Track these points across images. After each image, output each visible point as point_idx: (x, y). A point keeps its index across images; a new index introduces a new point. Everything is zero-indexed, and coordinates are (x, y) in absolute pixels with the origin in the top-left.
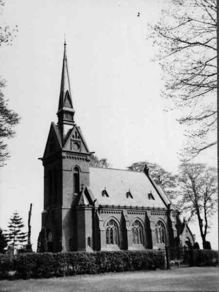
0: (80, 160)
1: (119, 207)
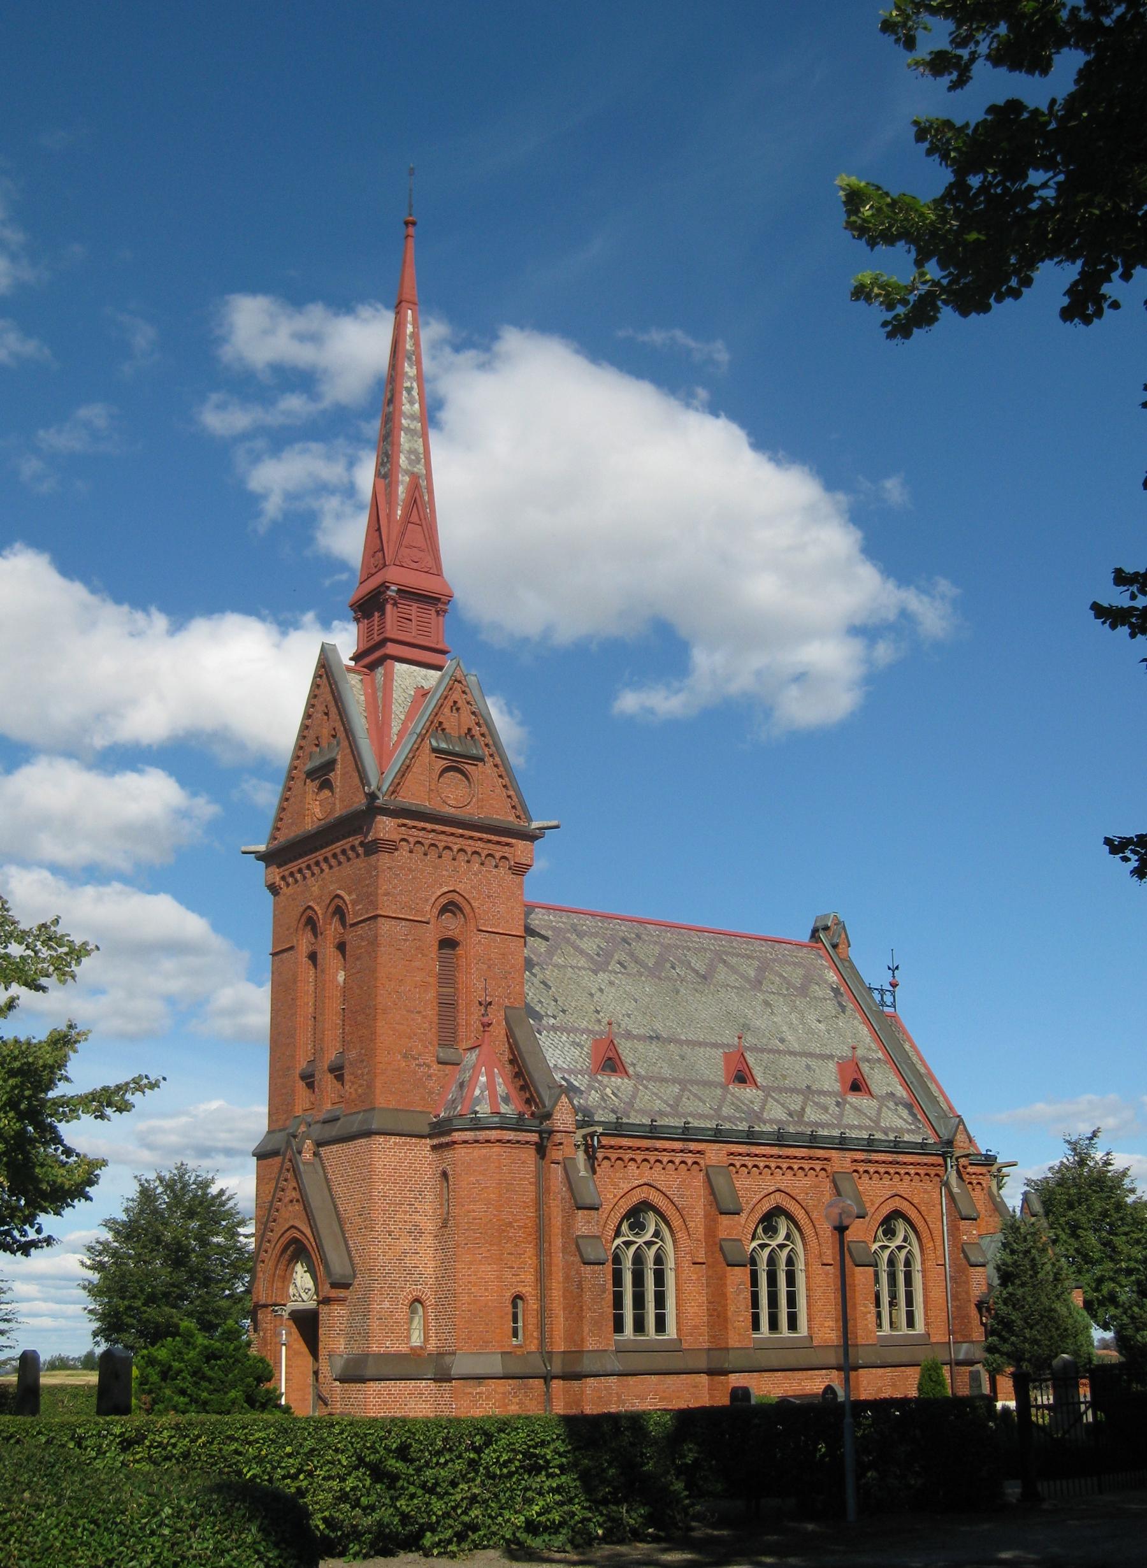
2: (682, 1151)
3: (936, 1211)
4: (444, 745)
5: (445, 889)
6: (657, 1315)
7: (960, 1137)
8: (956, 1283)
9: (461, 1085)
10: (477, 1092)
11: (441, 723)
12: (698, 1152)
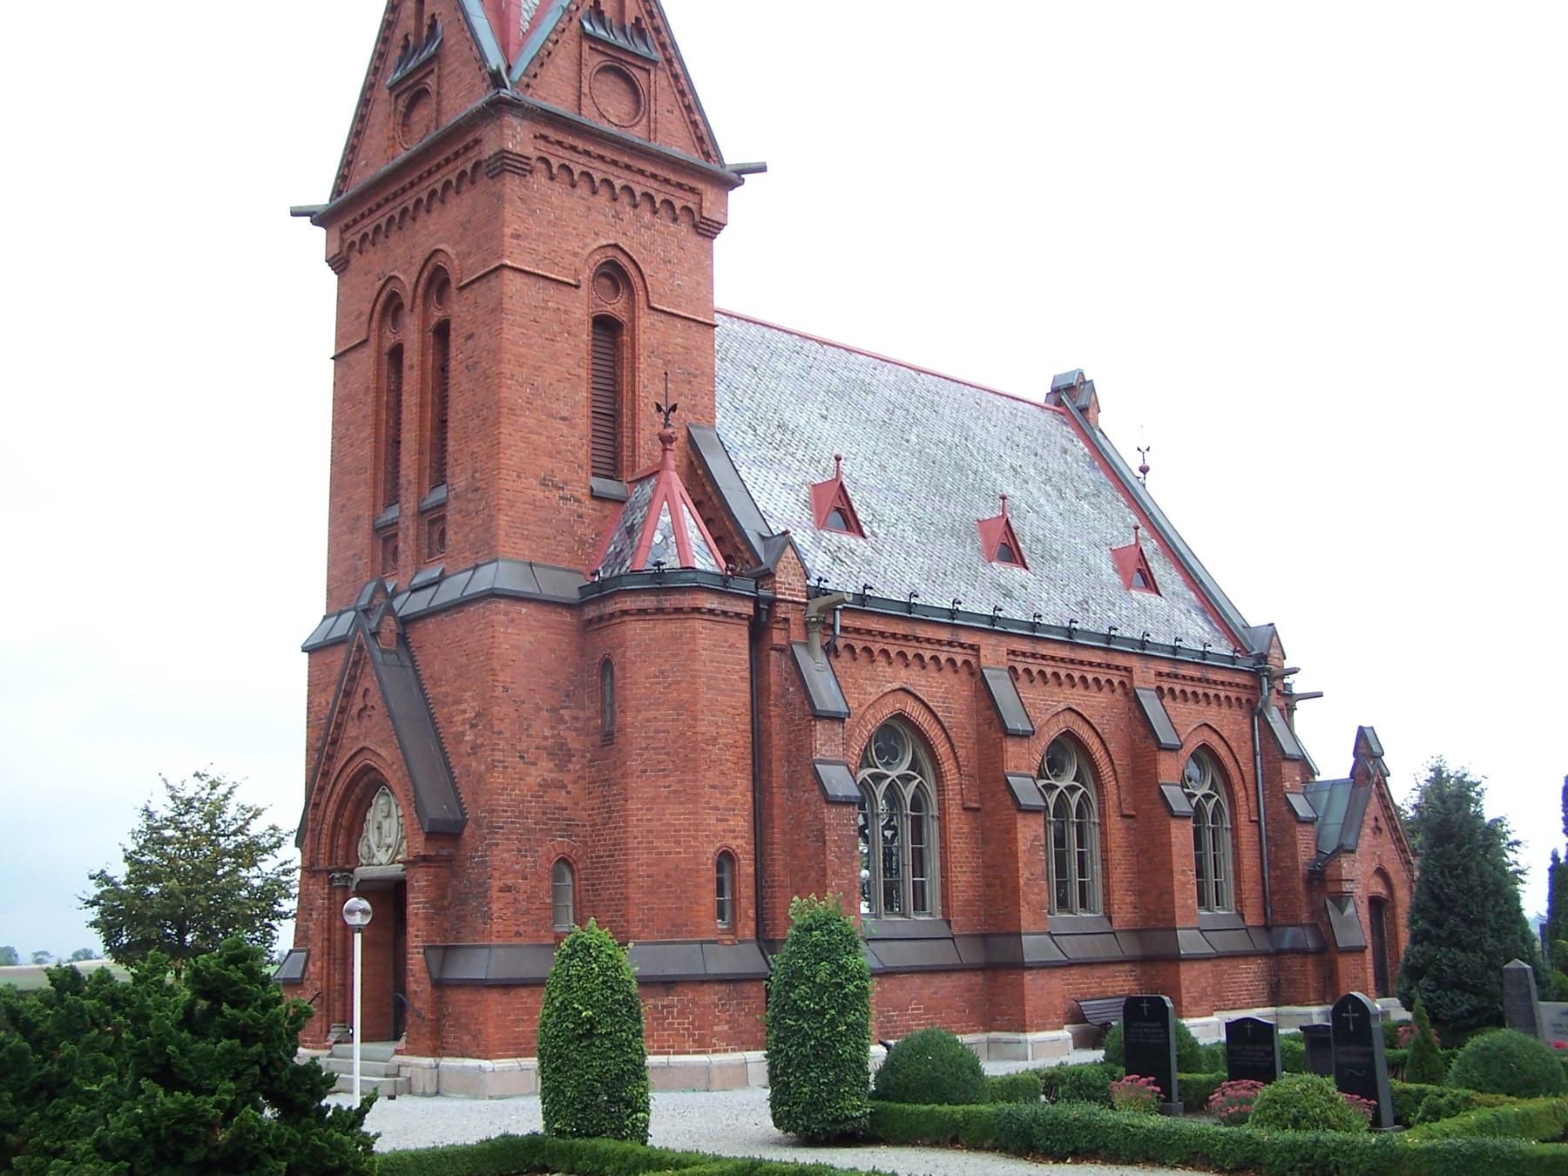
0: (583, 189)
1: (953, 617)
2: (950, 644)
4: (601, 33)
8: (1276, 845)
9: (630, 531)
10: (658, 538)
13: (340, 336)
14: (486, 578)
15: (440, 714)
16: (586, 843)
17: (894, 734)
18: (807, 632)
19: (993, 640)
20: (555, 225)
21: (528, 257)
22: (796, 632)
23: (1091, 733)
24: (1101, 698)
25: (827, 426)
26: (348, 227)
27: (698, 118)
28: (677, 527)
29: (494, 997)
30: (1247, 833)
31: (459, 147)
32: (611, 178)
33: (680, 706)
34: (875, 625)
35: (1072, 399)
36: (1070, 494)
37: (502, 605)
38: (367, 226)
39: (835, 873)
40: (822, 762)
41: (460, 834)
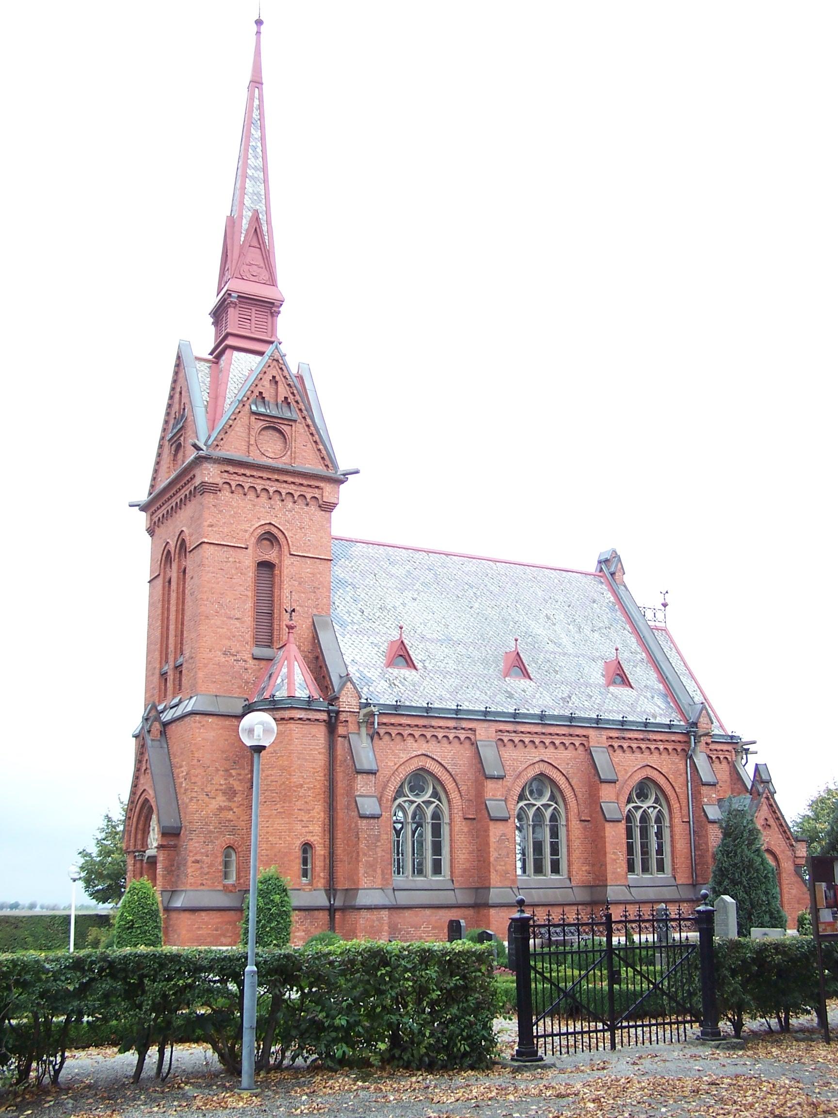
0: (251, 495)
3: (682, 779)
4: (262, 410)
5: (263, 522)
6: (552, 861)
7: (703, 720)
8: (699, 836)
10: (279, 681)
11: (261, 393)
12: (470, 729)
13: (152, 572)
14: (189, 706)
15: (176, 771)
16: (243, 838)
17: (418, 780)
18: (359, 727)
19: (486, 725)
20: (234, 517)
21: (218, 536)
22: (352, 727)
23: (559, 774)
24: (568, 754)
25: (415, 604)
26: (153, 513)
27: (321, 447)
28: (290, 675)
29: (187, 915)
30: (679, 828)
31: (188, 478)
32: (267, 487)
33: (283, 769)
34: (404, 721)
35: (608, 567)
36: (587, 630)
37: (198, 718)
38: (163, 510)
39: (365, 854)
40: (360, 796)
41: (179, 834)
